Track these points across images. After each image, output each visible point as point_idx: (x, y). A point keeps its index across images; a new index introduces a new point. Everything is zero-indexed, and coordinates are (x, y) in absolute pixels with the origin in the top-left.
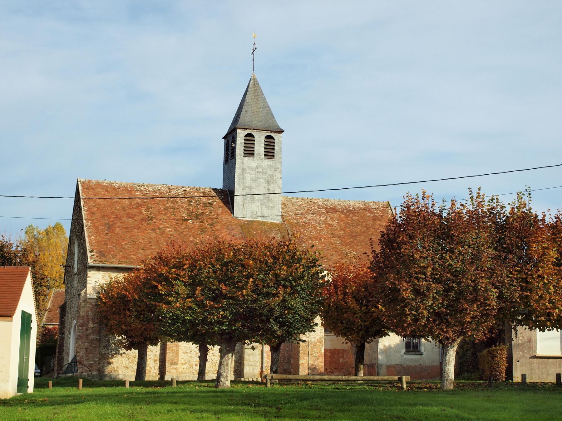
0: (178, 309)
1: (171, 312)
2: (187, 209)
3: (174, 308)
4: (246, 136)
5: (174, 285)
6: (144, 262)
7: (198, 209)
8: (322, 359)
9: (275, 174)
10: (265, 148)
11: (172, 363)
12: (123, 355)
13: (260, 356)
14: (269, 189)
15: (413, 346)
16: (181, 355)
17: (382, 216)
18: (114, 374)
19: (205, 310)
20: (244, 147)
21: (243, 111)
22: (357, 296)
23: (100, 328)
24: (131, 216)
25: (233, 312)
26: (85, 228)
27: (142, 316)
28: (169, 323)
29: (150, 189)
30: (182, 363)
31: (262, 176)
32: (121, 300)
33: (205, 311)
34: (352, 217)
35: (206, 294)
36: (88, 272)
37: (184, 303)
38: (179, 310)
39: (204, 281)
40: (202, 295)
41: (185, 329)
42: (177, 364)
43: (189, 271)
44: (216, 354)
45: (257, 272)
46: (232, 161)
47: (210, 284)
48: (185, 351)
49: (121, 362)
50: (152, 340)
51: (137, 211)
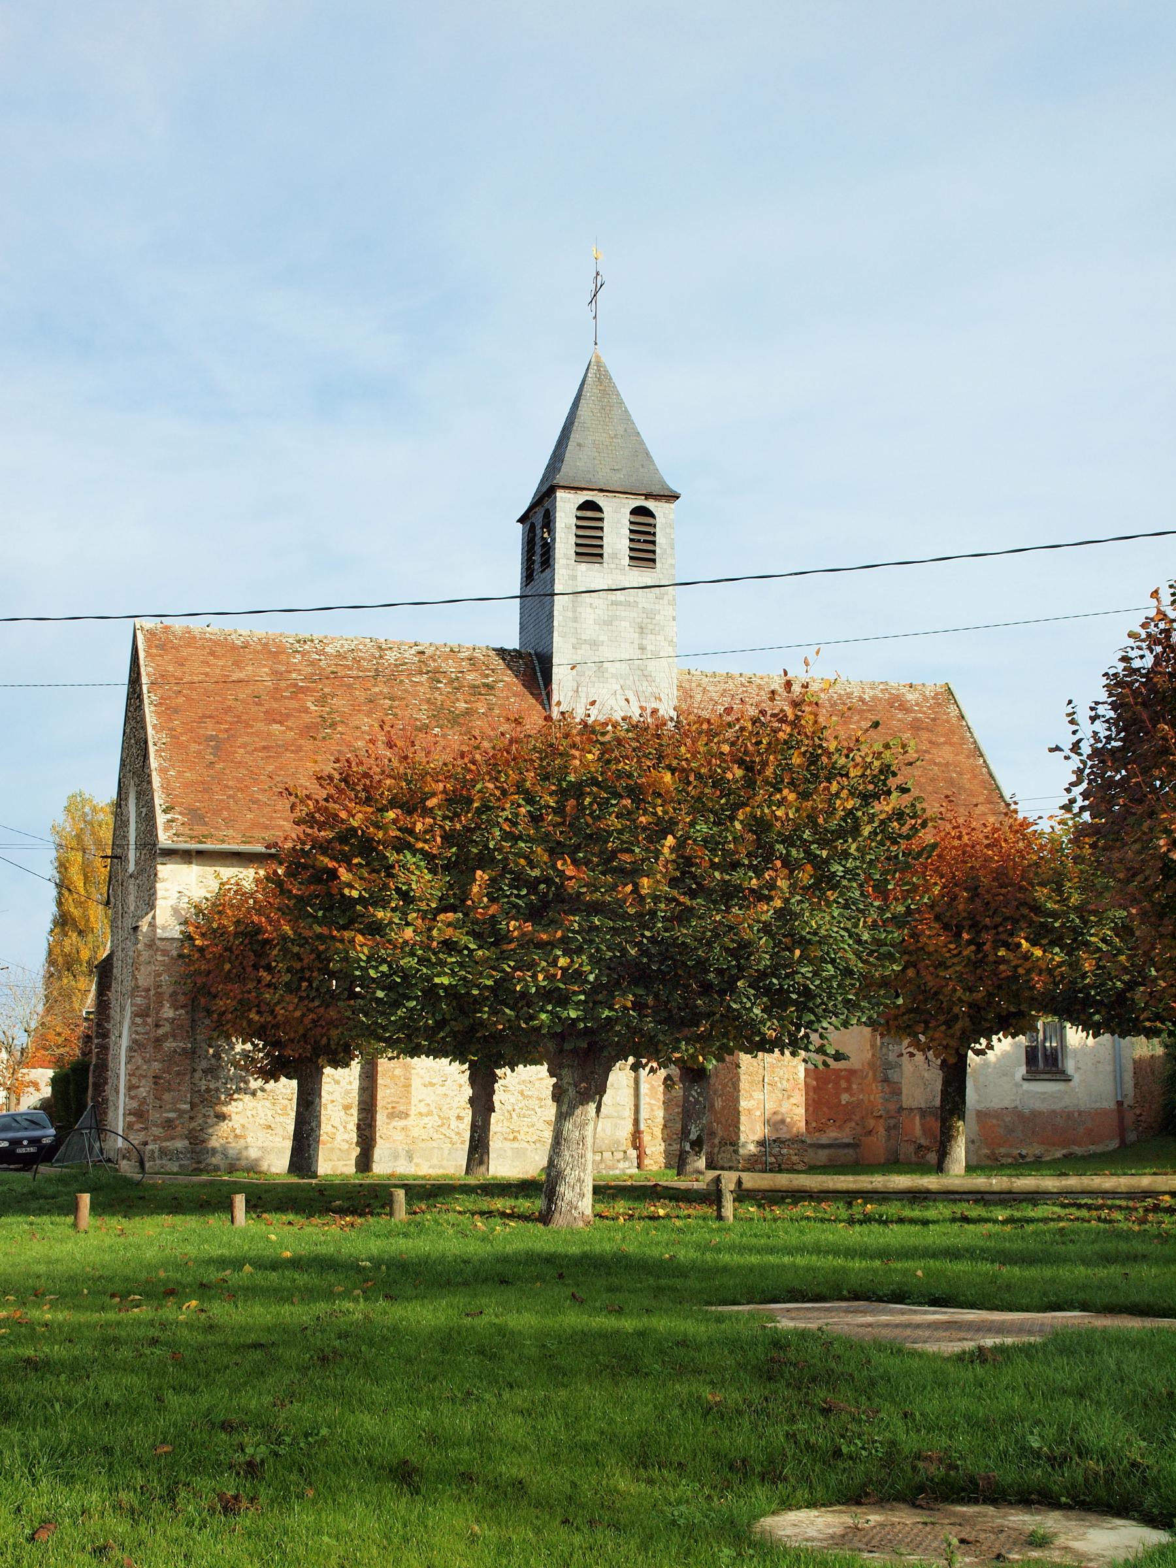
0: (407, 949)
1: (384, 961)
2: (428, 701)
3: (395, 947)
4: (580, 508)
5: (393, 867)
6: (290, 794)
7: (458, 700)
8: (799, 1098)
9: (657, 607)
10: (631, 540)
11: (392, 1113)
12: (259, 1093)
13: (632, 1091)
14: (642, 648)
15: (1045, 1056)
16: (418, 1091)
17: (934, 720)
18: (235, 1146)
19: (502, 952)
20: (577, 536)
21: (571, 446)
22: (948, 914)
23: (193, 1021)
24: (278, 718)
25: (601, 959)
26: (152, 750)
27: (305, 984)
28: (378, 1000)
29: (328, 649)
30: (420, 1114)
31: (623, 614)
32: (247, 941)
33: (503, 957)
34: (858, 722)
35: (507, 896)
36: (159, 867)
37: (430, 929)
38: (412, 954)
39: (499, 849)
40: (492, 900)
41: (436, 1021)
42: (407, 1115)
43: (445, 817)
44: (511, 1088)
45: (688, 814)
46: (544, 575)
47: (522, 861)
48: (427, 1080)
49: (254, 1112)
50: (335, 1053)
51: (294, 704)
